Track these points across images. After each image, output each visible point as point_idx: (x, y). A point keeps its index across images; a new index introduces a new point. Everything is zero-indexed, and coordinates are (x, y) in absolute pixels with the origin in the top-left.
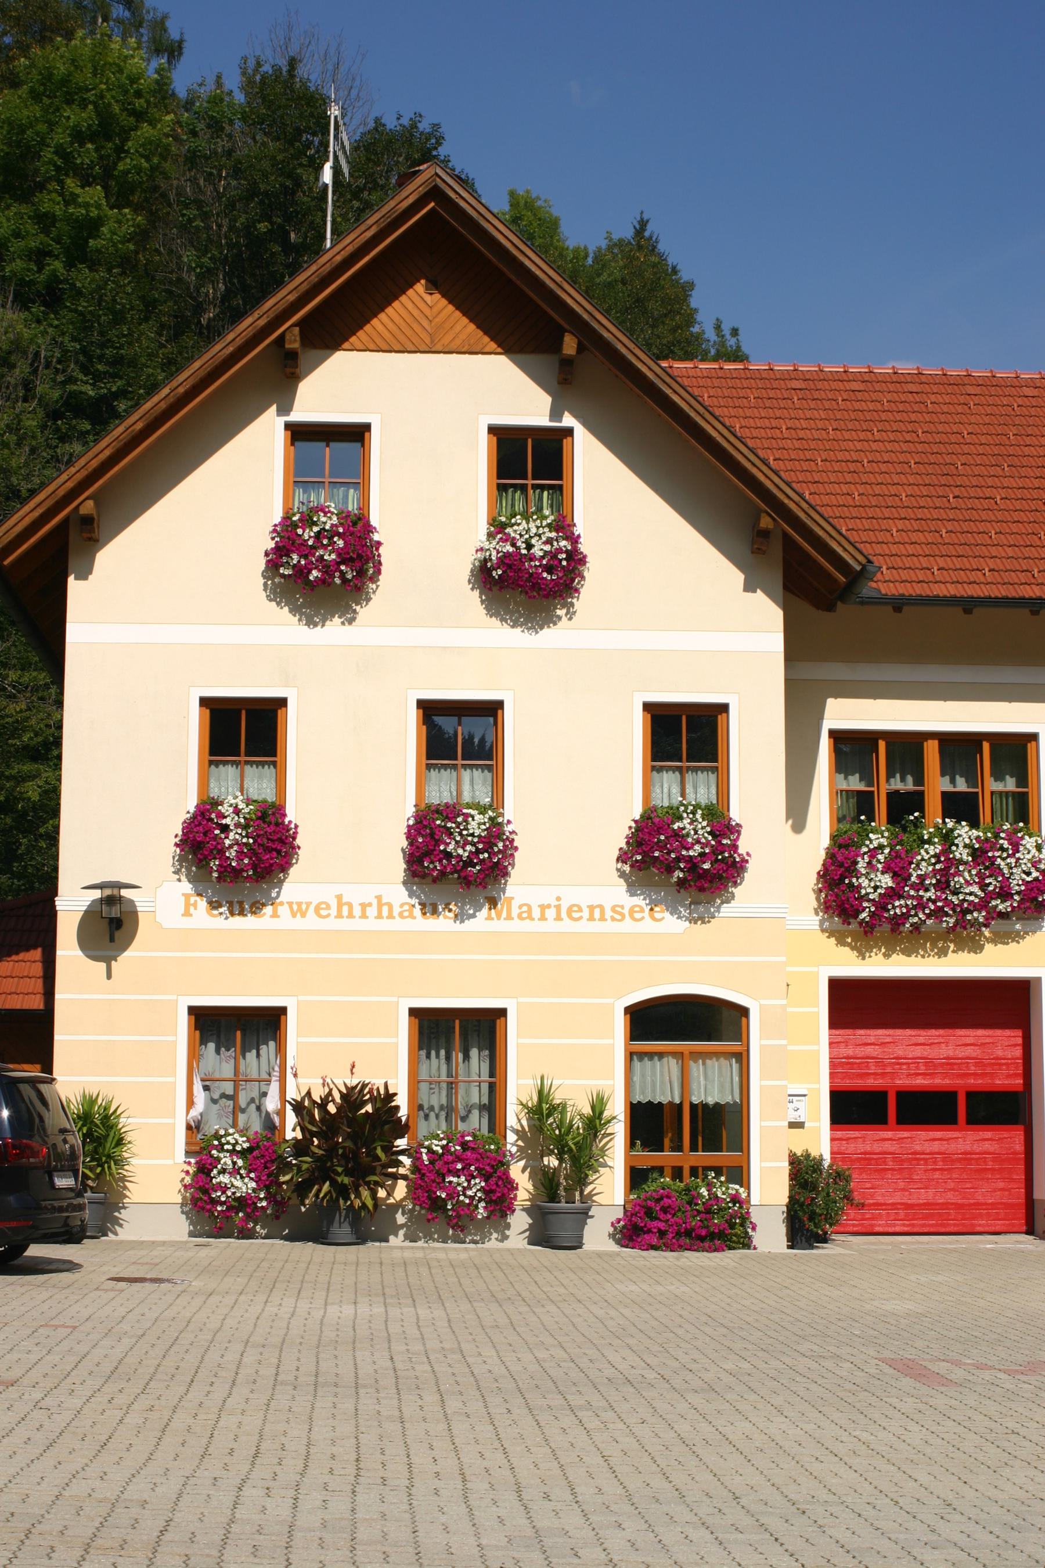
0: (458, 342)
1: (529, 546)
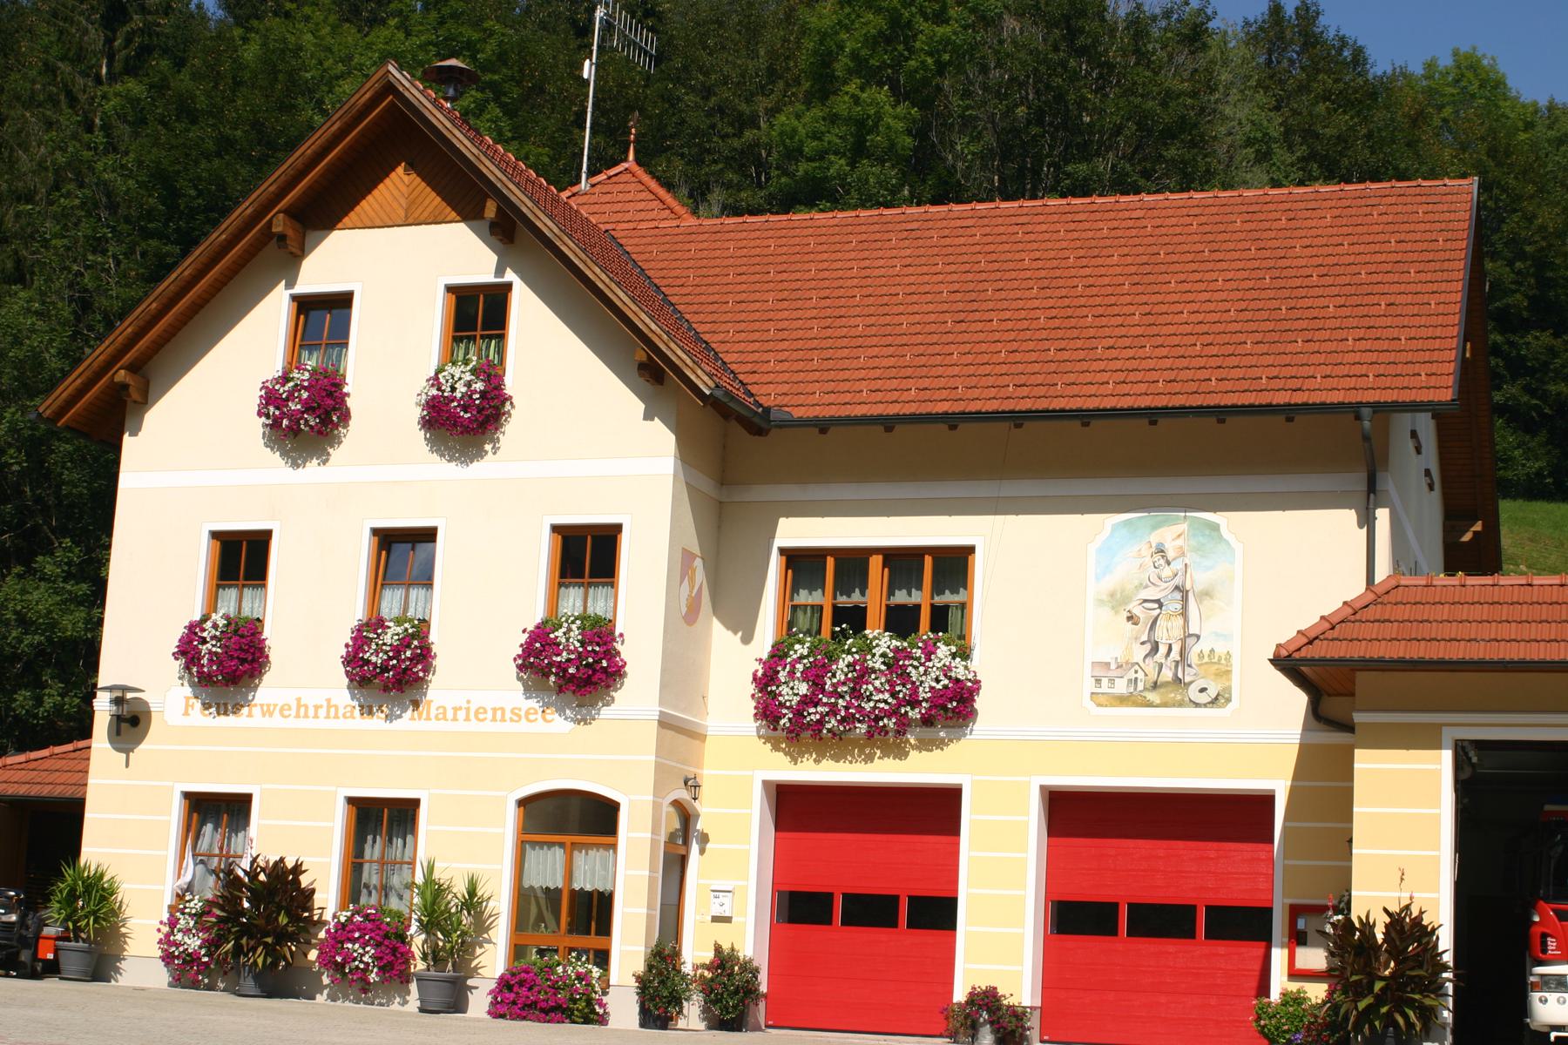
0: (426, 214)
1: (453, 389)
